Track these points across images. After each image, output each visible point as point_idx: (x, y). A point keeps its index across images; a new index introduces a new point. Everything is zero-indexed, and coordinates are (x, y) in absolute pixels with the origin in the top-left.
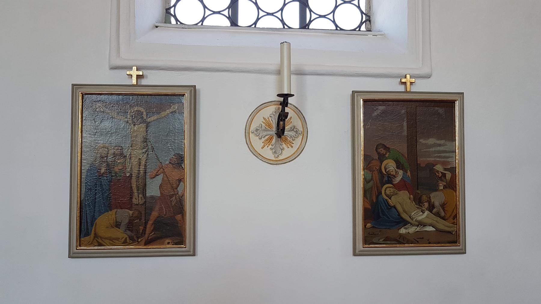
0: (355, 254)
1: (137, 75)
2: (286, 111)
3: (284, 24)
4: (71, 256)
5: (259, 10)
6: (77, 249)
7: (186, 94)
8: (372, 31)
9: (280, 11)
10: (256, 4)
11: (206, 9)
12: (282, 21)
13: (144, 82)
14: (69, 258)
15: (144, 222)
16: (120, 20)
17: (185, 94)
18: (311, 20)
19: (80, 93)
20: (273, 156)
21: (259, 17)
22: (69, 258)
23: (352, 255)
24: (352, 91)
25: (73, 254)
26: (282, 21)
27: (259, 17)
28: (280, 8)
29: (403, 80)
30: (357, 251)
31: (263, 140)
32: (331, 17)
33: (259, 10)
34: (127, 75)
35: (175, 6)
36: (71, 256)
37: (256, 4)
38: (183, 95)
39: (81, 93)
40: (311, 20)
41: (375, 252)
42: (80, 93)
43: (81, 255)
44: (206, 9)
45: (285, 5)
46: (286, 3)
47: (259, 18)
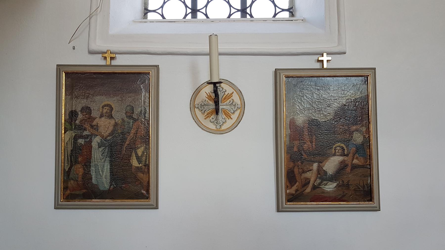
2: (213, 85)
3: (164, 18)
5: (231, 8)
7: (151, 72)
10: (228, 3)
11: (276, 7)
12: (162, 16)
15: (105, 162)
16: (338, 17)
17: (150, 73)
18: (231, 14)
19: (284, 76)
21: (276, 8)
24: (275, 69)
26: (162, 16)
29: (321, 59)
33: (231, 8)
35: (251, 6)
37: (228, 3)
40: (231, 14)
42: (284, 76)
43: (353, 209)
44: (187, 8)
45: (164, 3)
47: (187, 14)
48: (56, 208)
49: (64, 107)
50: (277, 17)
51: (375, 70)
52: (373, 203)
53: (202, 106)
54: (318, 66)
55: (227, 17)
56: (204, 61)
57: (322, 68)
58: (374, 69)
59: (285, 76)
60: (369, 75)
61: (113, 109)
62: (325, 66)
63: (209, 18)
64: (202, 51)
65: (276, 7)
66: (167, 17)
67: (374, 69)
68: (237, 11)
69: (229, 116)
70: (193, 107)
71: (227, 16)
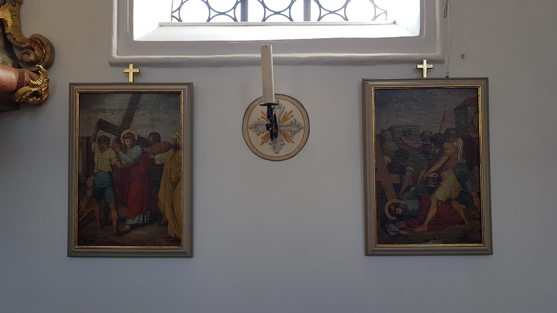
0: (71, 84)
1: (134, 73)
4: (71, 254)
5: (266, 9)
6: (376, 247)
7: (182, 91)
8: (398, 25)
9: (289, 9)
11: (266, 9)
13: (141, 80)
14: (68, 256)
17: (181, 92)
20: (274, 152)
21: (322, 9)
22: (68, 256)
23: (365, 255)
25: (72, 252)
27: (322, 9)
28: (263, 8)
29: (419, 66)
30: (369, 251)
31: (261, 136)
32: (342, 12)
33: (266, 9)
34: (124, 73)
36: (71, 254)
37: (207, 3)
38: (479, 87)
39: (78, 92)
41: (484, 252)
46: (178, 10)
48: (367, 254)
49: (479, 119)
50: (211, 21)
51: (486, 80)
52: (484, 245)
53: (256, 127)
54: (416, 76)
55: (206, 21)
56: (256, 73)
57: (420, 77)
58: (487, 79)
59: (374, 88)
60: (479, 87)
61: (150, 133)
62: (425, 76)
63: (348, 20)
64: (435, 56)
65: (266, 9)
66: (184, 20)
67: (487, 79)
68: (274, 13)
69: (289, 140)
70: (245, 128)
71: (262, 19)
